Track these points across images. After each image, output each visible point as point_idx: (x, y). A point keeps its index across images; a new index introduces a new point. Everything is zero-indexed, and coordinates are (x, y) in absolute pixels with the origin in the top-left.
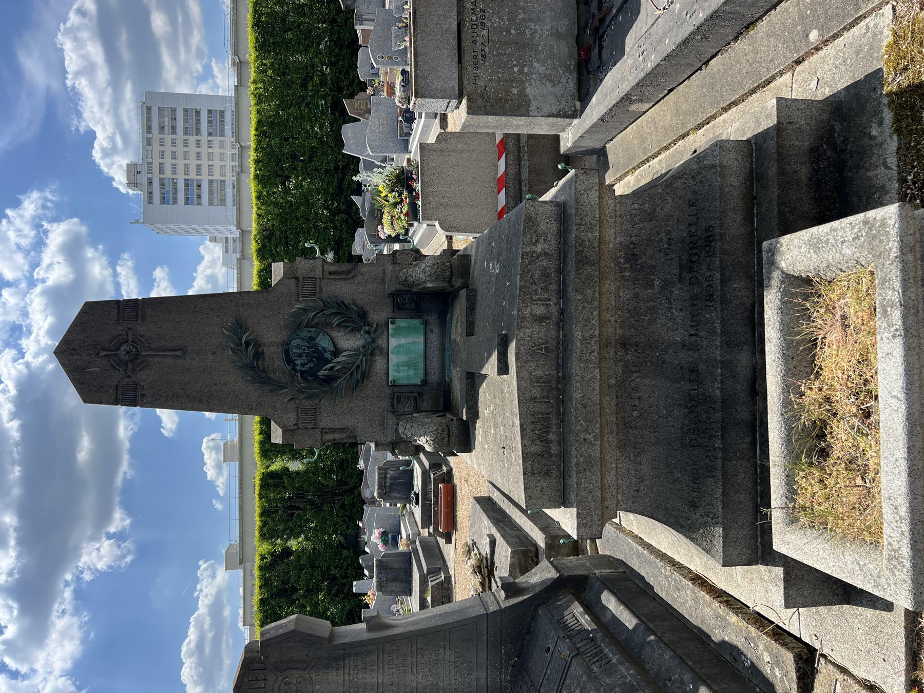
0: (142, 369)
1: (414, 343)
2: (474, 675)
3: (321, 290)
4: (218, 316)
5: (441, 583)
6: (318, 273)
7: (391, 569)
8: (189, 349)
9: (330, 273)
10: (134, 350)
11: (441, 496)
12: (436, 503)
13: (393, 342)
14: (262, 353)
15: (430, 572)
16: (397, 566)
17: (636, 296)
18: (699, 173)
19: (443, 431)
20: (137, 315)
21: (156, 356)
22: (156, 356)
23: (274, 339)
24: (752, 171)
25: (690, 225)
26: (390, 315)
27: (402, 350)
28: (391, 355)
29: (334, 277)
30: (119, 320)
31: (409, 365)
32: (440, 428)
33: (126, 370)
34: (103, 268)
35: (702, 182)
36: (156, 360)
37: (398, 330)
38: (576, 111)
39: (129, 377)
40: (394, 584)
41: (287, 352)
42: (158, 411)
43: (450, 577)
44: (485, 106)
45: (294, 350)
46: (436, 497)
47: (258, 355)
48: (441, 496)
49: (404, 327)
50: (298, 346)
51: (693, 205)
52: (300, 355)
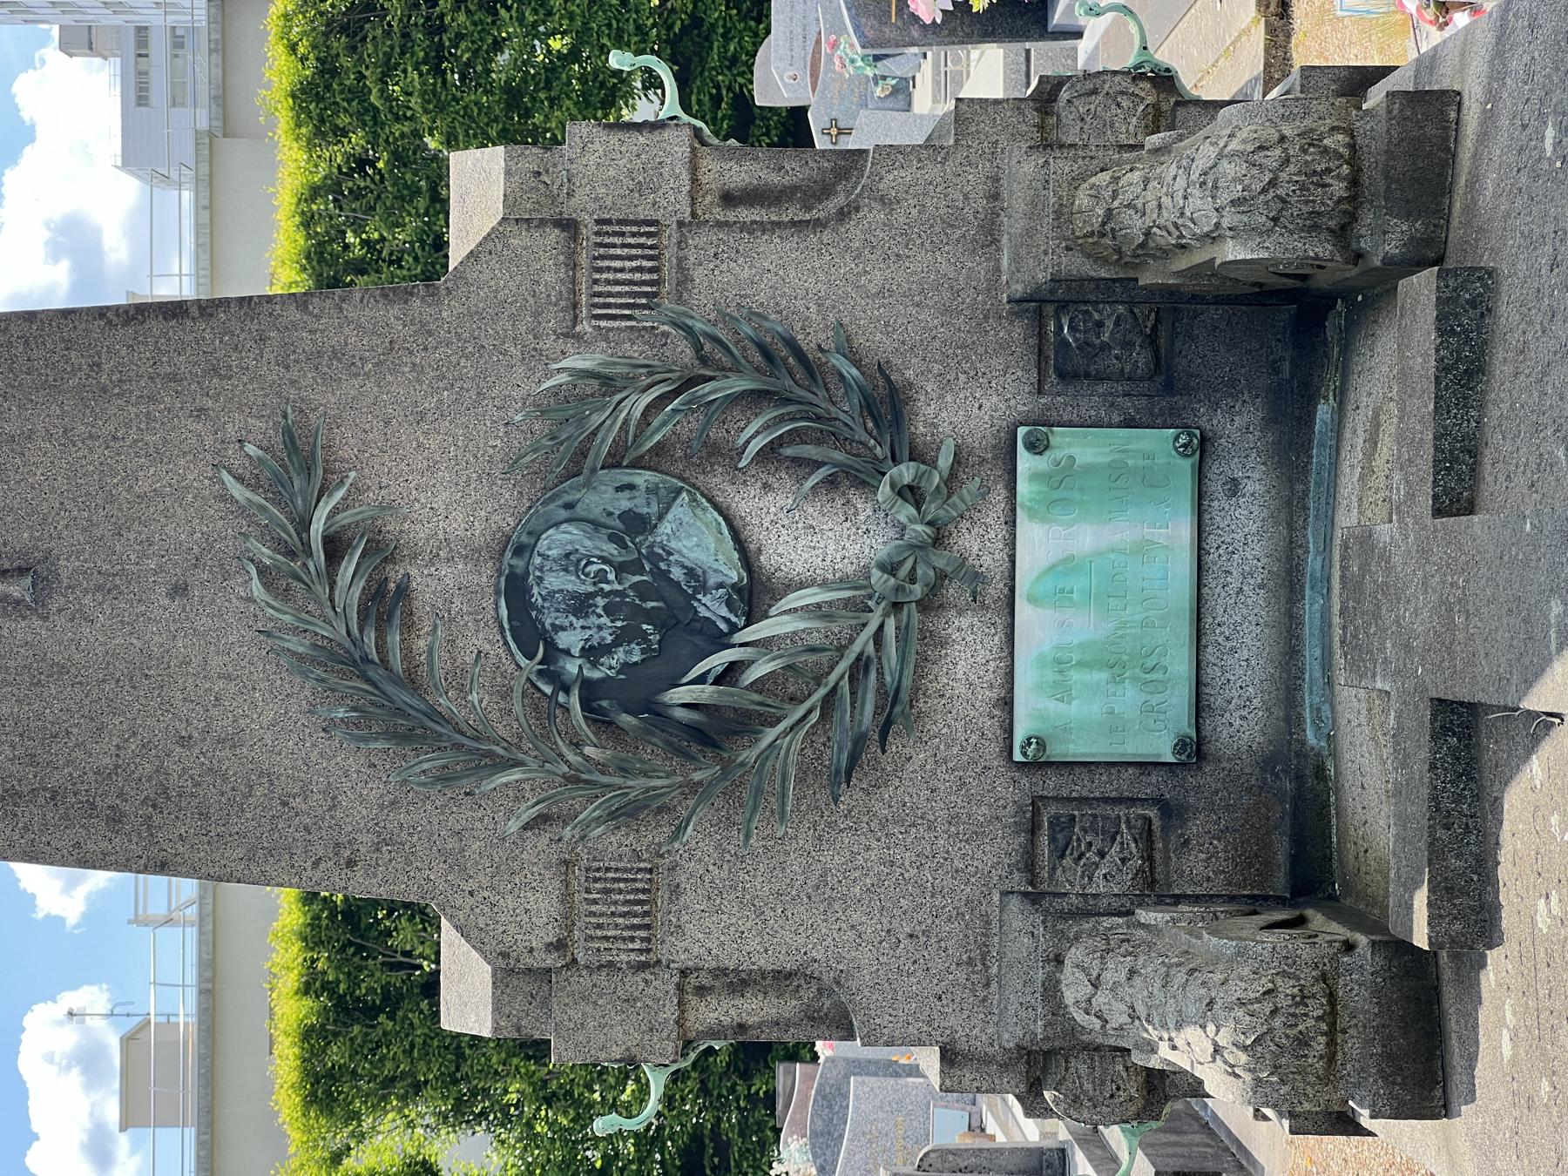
3: (684, 280)
8: (65, 567)
9: (729, 199)
13: (1038, 544)
14: (403, 591)
19: (1302, 999)
23: (456, 525)
26: (1023, 404)
27: (1078, 583)
41: (516, 589)
47: (386, 603)
49: (1090, 469)
50: (571, 561)
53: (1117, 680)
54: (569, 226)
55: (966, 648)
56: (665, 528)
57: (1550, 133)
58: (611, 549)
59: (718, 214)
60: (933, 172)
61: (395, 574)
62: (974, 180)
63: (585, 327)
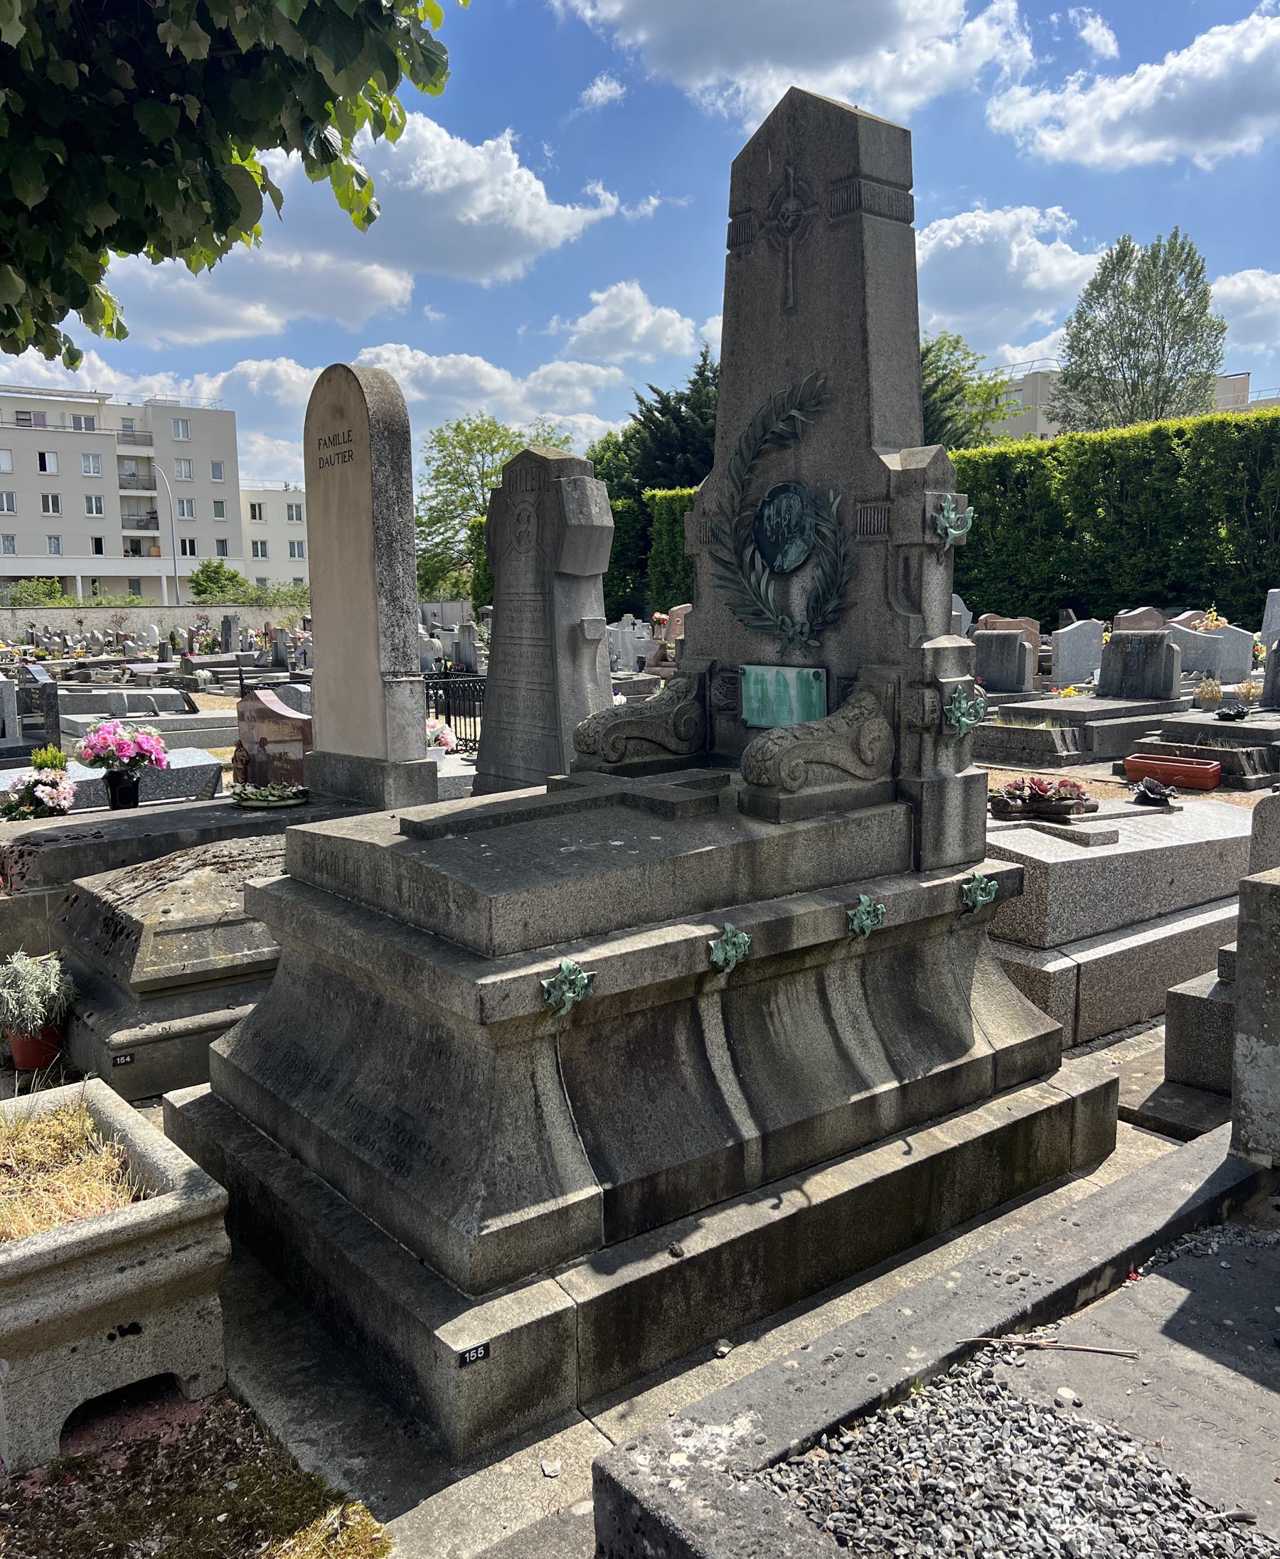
0: (771, 246)
1: (791, 711)
2: (522, 764)
3: (871, 544)
4: (835, 360)
5: (1053, 749)
6: (902, 538)
7: (1145, 662)
8: (793, 319)
9: (906, 559)
10: (789, 224)
11: (1195, 764)
12: (1187, 753)
13: (791, 674)
14: (785, 447)
15: (1086, 732)
16: (1149, 673)
17: (410, 1039)
18: (465, 1188)
19: (588, 746)
20: (838, 214)
21: (786, 263)
22: (786, 263)
23: (805, 464)
24: (443, 1273)
25: (430, 1148)
26: (835, 671)
27: (782, 688)
28: (775, 669)
29: (901, 566)
30: (833, 183)
31: (764, 699)
32: (590, 741)
33: (769, 218)
34: (470, 220)
35: (453, 1188)
36: (781, 265)
37: (804, 684)
38: (1248, 1151)
39: (762, 225)
40: (1119, 666)
41: (785, 489)
42: (920, 255)
43: (1060, 766)
44: (1260, 928)
45: (784, 502)
46: (1199, 754)
47: (782, 441)
48: (1195, 764)
49: (810, 694)
50: (790, 507)
51: (443, 1164)
52: (778, 513)
53: (759, 701)
54: (888, 497)
55: (770, 650)
56: (799, 542)
57: (618, 843)
58: (793, 522)
59: (902, 556)
60: (901, 639)
61: (791, 443)
62: (898, 655)
63: (859, 506)
